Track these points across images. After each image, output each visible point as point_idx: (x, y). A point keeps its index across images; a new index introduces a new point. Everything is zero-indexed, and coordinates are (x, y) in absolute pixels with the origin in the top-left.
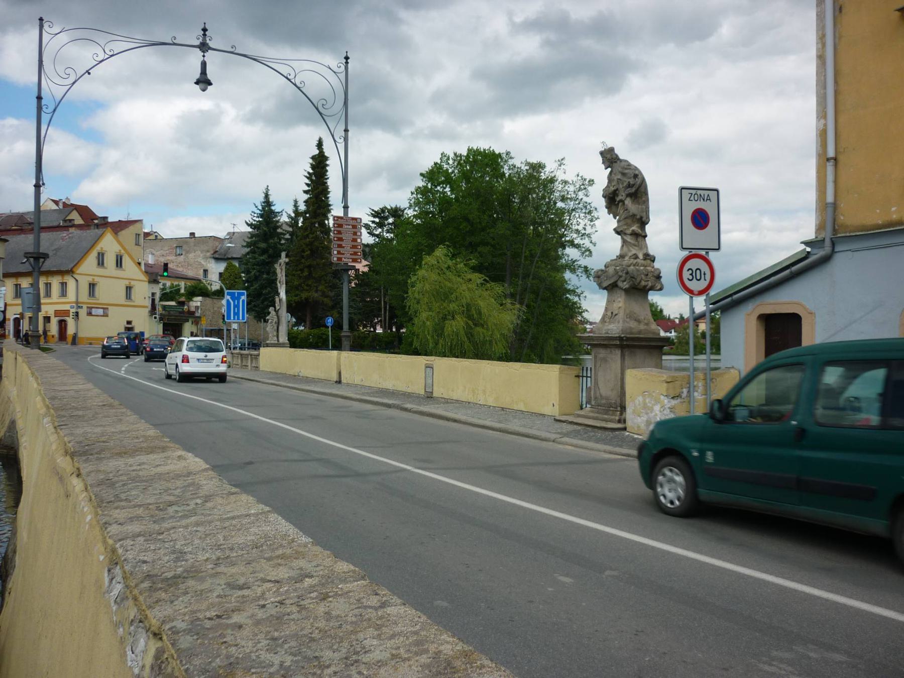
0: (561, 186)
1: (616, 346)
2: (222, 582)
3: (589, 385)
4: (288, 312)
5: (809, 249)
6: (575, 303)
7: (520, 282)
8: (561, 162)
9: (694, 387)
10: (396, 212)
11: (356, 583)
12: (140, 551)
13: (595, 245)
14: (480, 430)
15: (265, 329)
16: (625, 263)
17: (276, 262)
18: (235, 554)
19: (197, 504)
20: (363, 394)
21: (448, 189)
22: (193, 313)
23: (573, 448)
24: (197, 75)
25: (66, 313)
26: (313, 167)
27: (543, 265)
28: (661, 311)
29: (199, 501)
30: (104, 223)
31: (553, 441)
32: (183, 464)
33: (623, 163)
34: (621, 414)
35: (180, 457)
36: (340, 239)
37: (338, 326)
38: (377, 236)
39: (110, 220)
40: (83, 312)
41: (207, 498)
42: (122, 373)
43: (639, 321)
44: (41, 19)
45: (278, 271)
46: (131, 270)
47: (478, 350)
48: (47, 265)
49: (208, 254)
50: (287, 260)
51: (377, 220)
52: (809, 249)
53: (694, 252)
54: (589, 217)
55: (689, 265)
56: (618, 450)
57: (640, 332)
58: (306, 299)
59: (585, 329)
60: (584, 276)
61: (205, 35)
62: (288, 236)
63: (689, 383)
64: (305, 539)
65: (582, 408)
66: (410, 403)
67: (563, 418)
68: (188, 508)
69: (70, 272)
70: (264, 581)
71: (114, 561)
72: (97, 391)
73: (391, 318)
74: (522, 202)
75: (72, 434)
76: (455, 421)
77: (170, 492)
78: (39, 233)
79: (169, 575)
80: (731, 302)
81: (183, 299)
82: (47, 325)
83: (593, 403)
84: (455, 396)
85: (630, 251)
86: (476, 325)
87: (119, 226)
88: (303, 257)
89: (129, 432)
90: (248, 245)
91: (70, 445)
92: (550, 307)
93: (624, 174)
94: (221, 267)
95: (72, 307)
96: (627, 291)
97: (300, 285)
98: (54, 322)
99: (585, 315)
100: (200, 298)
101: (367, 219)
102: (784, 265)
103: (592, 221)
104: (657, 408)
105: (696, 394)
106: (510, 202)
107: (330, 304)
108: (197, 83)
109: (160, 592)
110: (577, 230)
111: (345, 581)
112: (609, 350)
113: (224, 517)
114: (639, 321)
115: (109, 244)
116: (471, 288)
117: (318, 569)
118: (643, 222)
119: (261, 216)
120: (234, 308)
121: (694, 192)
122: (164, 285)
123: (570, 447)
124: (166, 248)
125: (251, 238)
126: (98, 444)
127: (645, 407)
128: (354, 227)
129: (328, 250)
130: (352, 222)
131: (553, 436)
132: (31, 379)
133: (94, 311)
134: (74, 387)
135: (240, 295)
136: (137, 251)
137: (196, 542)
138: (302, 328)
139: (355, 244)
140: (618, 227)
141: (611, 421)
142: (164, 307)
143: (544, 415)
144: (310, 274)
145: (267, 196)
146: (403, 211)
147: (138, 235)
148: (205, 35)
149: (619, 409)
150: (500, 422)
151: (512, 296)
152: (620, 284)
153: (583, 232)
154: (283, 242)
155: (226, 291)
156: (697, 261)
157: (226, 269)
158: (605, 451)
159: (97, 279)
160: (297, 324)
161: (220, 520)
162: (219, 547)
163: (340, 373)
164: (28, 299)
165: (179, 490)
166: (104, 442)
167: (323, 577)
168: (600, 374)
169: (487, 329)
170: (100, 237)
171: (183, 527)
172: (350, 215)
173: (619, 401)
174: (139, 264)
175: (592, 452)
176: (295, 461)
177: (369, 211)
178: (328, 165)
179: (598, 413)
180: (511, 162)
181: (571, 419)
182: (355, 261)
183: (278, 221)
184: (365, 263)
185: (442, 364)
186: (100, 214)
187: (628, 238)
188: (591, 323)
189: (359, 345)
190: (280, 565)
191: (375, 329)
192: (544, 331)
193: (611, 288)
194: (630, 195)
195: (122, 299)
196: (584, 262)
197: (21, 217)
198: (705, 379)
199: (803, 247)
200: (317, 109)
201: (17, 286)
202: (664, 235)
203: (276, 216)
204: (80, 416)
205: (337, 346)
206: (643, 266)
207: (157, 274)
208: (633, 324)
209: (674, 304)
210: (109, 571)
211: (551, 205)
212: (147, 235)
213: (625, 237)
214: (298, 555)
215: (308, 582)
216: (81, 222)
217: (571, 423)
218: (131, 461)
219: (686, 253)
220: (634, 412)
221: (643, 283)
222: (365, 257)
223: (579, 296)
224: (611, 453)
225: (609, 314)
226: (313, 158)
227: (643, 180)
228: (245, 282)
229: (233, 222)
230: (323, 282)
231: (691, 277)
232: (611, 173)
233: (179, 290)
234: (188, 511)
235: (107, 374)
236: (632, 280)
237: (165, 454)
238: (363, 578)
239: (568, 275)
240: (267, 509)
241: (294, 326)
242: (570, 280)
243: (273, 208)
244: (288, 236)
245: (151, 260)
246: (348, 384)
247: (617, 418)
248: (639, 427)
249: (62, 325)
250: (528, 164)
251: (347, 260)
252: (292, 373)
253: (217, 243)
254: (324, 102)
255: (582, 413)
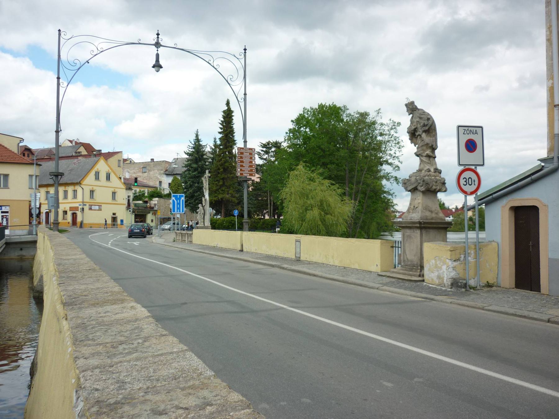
0: (379, 126)
1: (417, 227)
2: (148, 408)
3: (400, 252)
4: (210, 206)
5: (543, 164)
6: (389, 200)
7: (355, 187)
8: (378, 111)
9: (469, 253)
10: (277, 145)
11: (243, 412)
12: (96, 381)
13: (401, 163)
14: (330, 282)
15: (196, 217)
16: (422, 175)
17: (203, 176)
18: (160, 385)
19: (139, 343)
20: (257, 258)
21: (308, 130)
22: (153, 208)
23: (390, 293)
24: (154, 62)
25: (77, 209)
26: (224, 117)
27: (369, 176)
28: (444, 204)
29: (140, 341)
30: (99, 154)
31: (377, 289)
32: (133, 312)
33: (420, 111)
34: (421, 271)
35: (132, 307)
36: (242, 162)
37: (241, 215)
38: (265, 159)
39: (103, 152)
40: (86, 208)
41: (146, 339)
42: (109, 246)
43: (431, 212)
44: (59, 31)
45: (204, 182)
46: (116, 183)
47: (330, 231)
48: (63, 180)
49: (162, 172)
50: (209, 175)
51: (264, 149)
52: (543, 164)
53: (467, 167)
54: (398, 146)
55: (463, 176)
56: (419, 294)
57: (432, 219)
58: (222, 199)
59: (395, 216)
60: (395, 183)
61: (158, 37)
62: (210, 160)
63: (465, 251)
64: (210, 373)
65: (395, 267)
66: (286, 264)
67: (384, 274)
68: (132, 346)
69: (79, 183)
70: (178, 408)
71: (79, 387)
72: (88, 259)
73: (274, 210)
74: (355, 137)
75: (66, 290)
76: (314, 275)
77: (122, 333)
78: (58, 160)
79: (112, 401)
80: (492, 198)
81: (146, 199)
82: (65, 216)
83: (402, 264)
84: (314, 259)
85: (425, 167)
86: (327, 214)
87: (108, 156)
88: (219, 173)
89: (102, 288)
90: (186, 166)
91: (63, 298)
92: (374, 202)
93: (420, 118)
94: (170, 179)
95: (80, 205)
96: (424, 193)
97: (217, 190)
98: (69, 213)
99: (396, 207)
100: (157, 199)
101: (258, 149)
102: (527, 175)
103: (399, 148)
104: (444, 267)
105: (469, 258)
106: (347, 136)
107: (236, 201)
108: (153, 67)
109: (104, 415)
110: (390, 154)
111: (234, 409)
112: (412, 230)
113: (156, 354)
114: (431, 212)
115: (102, 166)
116: (325, 191)
117: (216, 398)
118: (433, 148)
119: (194, 148)
120: (177, 205)
121: (466, 128)
122: (135, 191)
123: (388, 293)
124: (136, 169)
125: (188, 161)
126: (81, 298)
127: (436, 266)
128: (251, 154)
129: (234, 168)
130: (249, 151)
131: (377, 285)
132: (51, 251)
133: (93, 207)
134: (74, 257)
135: (181, 197)
136: (119, 171)
137: (135, 373)
138: (219, 217)
139: (251, 164)
140: (417, 152)
141: (414, 276)
142: (135, 205)
143: (371, 272)
144: (224, 183)
145: (197, 136)
146: (281, 144)
147: (119, 161)
148: (158, 37)
149: (419, 268)
150: (343, 276)
151: (350, 195)
152: (419, 188)
153: (394, 155)
154: (207, 164)
155: (172, 195)
156: (469, 175)
157: (173, 181)
158: (411, 296)
159: (95, 188)
160: (216, 214)
161: (152, 356)
162: (149, 378)
163: (242, 245)
164: (52, 200)
165: (128, 333)
166: (85, 296)
167: (220, 405)
168: (407, 245)
169: (334, 216)
170: (96, 163)
171: (127, 361)
172: (249, 146)
173: (419, 263)
174: (120, 178)
175: (402, 296)
176: (215, 302)
177: (259, 144)
178: (233, 116)
179: (405, 270)
180: (348, 112)
181: (388, 274)
182: (251, 175)
183: (204, 151)
184: (257, 176)
185: (307, 240)
186: (97, 148)
187: (424, 159)
188: (399, 212)
189: (254, 228)
190: (190, 394)
191: (264, 217)
192: (370, 218)
193: (414, 190)
194: (425, 131)
195: (110, 200)
196: (394, 174)
197: (50, 150)
198: (475, 249)
199: (539, 162)
200: (227, 81)
201: (47, 192)
202: (448, 155)
203: (203, 148)
204: (73, 277)
205: (241, 228)
206: (434, 176)
207: (131, 184)
208: (428, 214)
209: (453, 200)
210: (76, 392)
211: (373, 138)
212: (125, 160)
213: (422, 158)
214: (204, 386)
215: (209, 409)
216: (86, 153)
217: (388, 277)
218: (100, 309)
219: (462, 168)
220: (429, 270)
221: (434, 187)
222: (257, 171)
223: (392, 195)
224: (415, 296)
225: (412, 207)
226: (224, 112)
227: (433, 122)
228: (184, 189)
229: (177, 151)
230: (231, 188)
231: (465, 183)
232: (412, 117)
233: (144, 194)
234: (132, 349)
235: (100, 246)
236: (427, 185)
237: (123, 305)
238: (248, 407)
239: (384, 182)
240: (185, 348)
241: (214, 215)
242: (385, 185)
243: (201, 143)
244: (210, 160)
245: (127, 176)
246: (247, 252)
247: (418, 274)
248: (432, 279)
249: (74, 216)
250: (358, 113)
251: (246, 174)
252: (212, 245)
253: (167, 165)
254: (231, 77)
255: (395, 270)
